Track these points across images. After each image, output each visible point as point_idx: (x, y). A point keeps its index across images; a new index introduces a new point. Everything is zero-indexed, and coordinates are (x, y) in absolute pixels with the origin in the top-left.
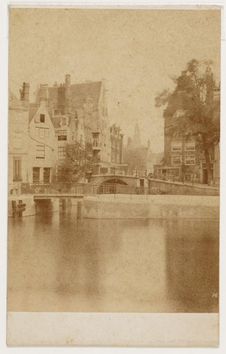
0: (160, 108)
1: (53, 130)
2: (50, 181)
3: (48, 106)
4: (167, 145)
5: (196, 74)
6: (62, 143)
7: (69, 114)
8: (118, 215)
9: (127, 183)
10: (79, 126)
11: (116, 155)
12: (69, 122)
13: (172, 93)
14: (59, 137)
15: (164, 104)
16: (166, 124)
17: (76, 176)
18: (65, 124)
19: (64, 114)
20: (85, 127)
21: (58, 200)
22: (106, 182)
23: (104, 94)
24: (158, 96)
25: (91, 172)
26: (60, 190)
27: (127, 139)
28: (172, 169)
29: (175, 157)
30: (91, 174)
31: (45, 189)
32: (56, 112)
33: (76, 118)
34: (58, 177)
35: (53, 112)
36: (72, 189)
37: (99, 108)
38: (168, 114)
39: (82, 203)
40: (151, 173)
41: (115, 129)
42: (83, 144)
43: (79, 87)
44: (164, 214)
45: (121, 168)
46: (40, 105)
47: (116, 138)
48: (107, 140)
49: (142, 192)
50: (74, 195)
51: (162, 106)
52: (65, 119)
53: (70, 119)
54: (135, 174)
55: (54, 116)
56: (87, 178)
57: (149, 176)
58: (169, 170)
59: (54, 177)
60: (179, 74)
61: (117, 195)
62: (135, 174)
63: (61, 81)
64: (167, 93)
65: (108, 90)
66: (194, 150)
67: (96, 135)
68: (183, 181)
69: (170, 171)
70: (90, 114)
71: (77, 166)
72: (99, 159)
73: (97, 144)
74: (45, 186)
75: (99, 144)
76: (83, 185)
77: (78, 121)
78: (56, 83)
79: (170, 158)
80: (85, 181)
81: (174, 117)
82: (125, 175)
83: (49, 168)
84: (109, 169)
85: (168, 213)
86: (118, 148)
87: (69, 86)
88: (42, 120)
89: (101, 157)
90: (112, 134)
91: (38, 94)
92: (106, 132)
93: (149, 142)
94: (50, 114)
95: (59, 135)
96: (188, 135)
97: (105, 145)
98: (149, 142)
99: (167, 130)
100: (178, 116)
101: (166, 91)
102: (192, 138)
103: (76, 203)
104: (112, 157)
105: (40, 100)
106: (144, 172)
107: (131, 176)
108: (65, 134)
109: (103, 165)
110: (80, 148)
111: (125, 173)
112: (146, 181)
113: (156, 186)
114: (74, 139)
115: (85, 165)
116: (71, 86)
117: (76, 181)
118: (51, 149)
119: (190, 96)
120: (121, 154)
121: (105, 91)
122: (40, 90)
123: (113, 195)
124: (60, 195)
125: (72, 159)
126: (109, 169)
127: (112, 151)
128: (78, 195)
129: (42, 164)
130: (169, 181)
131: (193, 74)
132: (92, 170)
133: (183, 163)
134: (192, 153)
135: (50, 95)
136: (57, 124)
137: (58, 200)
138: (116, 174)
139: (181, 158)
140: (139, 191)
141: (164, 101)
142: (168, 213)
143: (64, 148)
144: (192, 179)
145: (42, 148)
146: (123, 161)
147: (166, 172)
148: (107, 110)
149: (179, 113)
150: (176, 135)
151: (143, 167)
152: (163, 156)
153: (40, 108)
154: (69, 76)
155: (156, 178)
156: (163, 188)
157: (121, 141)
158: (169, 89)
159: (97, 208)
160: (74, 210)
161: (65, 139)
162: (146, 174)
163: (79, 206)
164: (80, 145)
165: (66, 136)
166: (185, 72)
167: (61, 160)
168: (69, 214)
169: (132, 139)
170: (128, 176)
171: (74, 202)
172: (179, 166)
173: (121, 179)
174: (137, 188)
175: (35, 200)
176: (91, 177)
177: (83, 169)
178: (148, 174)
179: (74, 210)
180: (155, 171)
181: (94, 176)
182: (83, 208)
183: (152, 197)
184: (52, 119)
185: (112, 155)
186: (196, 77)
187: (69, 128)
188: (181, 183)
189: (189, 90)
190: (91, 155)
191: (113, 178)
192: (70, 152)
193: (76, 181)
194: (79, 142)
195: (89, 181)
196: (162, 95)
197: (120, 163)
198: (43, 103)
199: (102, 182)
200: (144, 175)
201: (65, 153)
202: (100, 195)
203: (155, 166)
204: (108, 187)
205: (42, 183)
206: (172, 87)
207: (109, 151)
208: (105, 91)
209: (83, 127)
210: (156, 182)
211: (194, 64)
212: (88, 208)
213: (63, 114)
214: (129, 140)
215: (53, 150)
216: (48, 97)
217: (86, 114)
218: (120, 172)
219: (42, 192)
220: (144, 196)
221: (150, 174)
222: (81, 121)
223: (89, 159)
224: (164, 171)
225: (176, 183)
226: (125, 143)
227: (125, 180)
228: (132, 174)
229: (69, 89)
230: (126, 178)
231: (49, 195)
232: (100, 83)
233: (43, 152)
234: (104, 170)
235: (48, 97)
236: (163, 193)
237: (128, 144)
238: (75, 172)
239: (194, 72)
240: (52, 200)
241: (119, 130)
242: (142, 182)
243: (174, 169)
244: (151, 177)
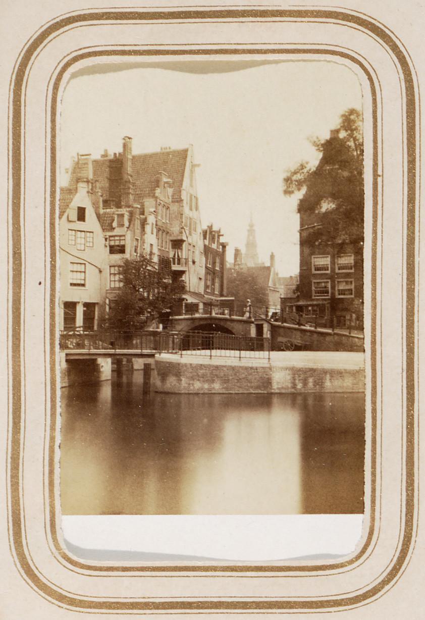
0: (292, 195)
1: (99, 235)
2: (96, 328)
3: (91, 192)
4: (305, 263)
5: (355, 134)
6: (117, 258)
7: (129, 207)
8: (217, 386)
9: (234, 331)
10: (148, 228)
11: (213, 284)
12: (130, 221)
13: (314, 169)
14: (111, 247)
15: (299, 190)
16: (302, 225)
17: (143, 317)
18: (123, 225)
19: (120, 207)
20: (159, 230)
21: (109, 360)
22: (196, 328)
23: (192, 172)
24: (289, 174)
25: (168, 310)
26: (112, 344)
27: (233, 252)
28: (312, 306)
29: (318, 283)
30: (168, 314)
31: (86, 342)
32: (106, 203)
33: (143, 213)
34: (110, 319)
35: (101, 205)
36: (134, 342)
37: (184, 196)
38: (306, 208)
39: (153, 367)
40: (276, 313)
41: (211, 234)
42: (155, 259)
43: (143, 159)
44: (300, 386)
45: (223, 304)
46: (77, 188)
47: (214, 253)
48: (197, 253)
49: (260, 348)
50: (138, 351)
51: (296, 192)
52: (122, 215)
53: (131, 214)
54: (247, 314)
55: (102, 211)
56: (162, 322)
57: (272, 317)
58: (307, 306)
59: (102, 320)
60: (326, 136)
61: (214, 352)
62: (247, 314)
63: (116, 149)
64: (305, 171)
65: (198, 165)
66: (353, 271)
67: (177, 244)
68: (332, 326)
69: (310, 308)
70: (168, 208)
71: (142, 299)
72: (183, 287)
73: (179, 260)
74: (86, 335)
75: (183, 261)
76: (155, 334)
77: (145, 220)
78: (106, 151)
79: (310, 284)
80: (158, 328)
81: (317, 212)
82: (230, 315)
83: (94, 304)
84: (201, 306)
85: (305, 383)
86: (217, 268)
87: (130, 157)
88: (81, 214)
89: (187, 285)
90: (207, 242)
91: (74, 172)
92: (195, 241)
93: (272, 257)
94: (97, 209)
95: (112, 243)
96: (343, 244)
97: (194, 262)
98: (272, 257)
99: (305, 234)
100: (323, 210)
101: (302, 167)
102: (349, 248)
103: (142, 367)
104: (206, 283)
105: (78, 180)
106: (263, 310)
107: (241, 318)
108: (122, 243)
109: (190, 300)
110: (149, 268)
111: (230, 311)
112: (266, 328)
113: (285, 336)
114: (139, 251)
115: (158, 297)
116: (134, 157)
117: (142, 328)
118: (97, 271)
119: (346, 174)
120: (222, 278)
121: (193, 166)
122: (78, 163)
123: (208, 352)
124: (112, 351)
125: (134, 287)
126: (201, 306)
127: (207, 273)
128: (145, 352)
129: (81, 296)
130: (308, 327)
131: (351, 136)
132: (170, 308)
133: (333, 294)
134: (348, 275)
135: (95, 174)
136: (106, 224)
137: (109, 360)
138: (214, 315)
139: (329, 285)
140: (256, 345)
141: (300, 184)
142: (305, 383)
143: (119, 266)
144: (348, 323)
145: (82, 268)
146: (225, 293)
147: (302, 311)
148: (197, 199)
149: (326, 206)
150: (320, 244)
151: (261, 301)
152: (296, 282)
153: (78, 194)
154: (130, 138)
155: (284, 321)
156: (297, 340)
157: (222, 255)
158: (307, 163)
159: (178, 375)
160: (138, 378)
161: (121, 250)
162: (267, 315)
163: (147, 369)
164: (149, 262)
165: (124, 246)
166: (337, 131)
167: (114, 289)
168: (130, 384)
169: (243, 251)
170: (235, 317)
171: (139, 363)
172: (325, 300)
173: (222, 324)
174: (251, 339)
175: (67, 361)
176: (168, 320)
177: (152, 304)
178: (270, 314)
179: (138, 378)
180: (282, 310)
181: (177, 317)
182: (154, 373)
183: (275, 355)
184: (99, 216)
185: (206, 280)
186: (355, 139)
187: (129, 232)
188: (330, 331)
189: (344, 164)
190: (168, 280)
191: (209, 322)
192: (132, 273)
193: (145, 323)
194: (148, 257)
195: (164, 328)
196: (295, 173)
197: (222, 295)
198: (83, 188)
199: (186, 329)
200: (263, 317)
201: (121, 277)
202: (184, 352)
203: (284, 301)
204: (198, 337)
205: (80, 331)
206: (313, 159)
207: (202, 272)
208: (193, 166)
209: (155, 230)
210: (284, 327)
211: (352, 117)
212: (164, 376)
213: (119, 206)
214: (237, 253)
215: (100, 271)
216: (91, 177)
217: (160, 208)
218: (221, 311)
219: (79, 346)
220: (265, 354)
221: (275, 314)
222: (151, 219)
223: (165, 287)
224: (300, 309)
225: (319, 330)
226: (230, 258)
227: (229, 325)
228: (243, 315)
229: (129, 163)
230: (233, 321)
231: (93, 351)
232: (186, 151)
233: (83, 274)
234: (192, 308)
235: (91, 177)
236: (298, 348)
237: (235, 262)
238: (141, 312)
239: (352, 130)
240: (100, 361)
241: (219, 236)
242: (260, 328)
243: (317, 305)
244: (276, 320)
